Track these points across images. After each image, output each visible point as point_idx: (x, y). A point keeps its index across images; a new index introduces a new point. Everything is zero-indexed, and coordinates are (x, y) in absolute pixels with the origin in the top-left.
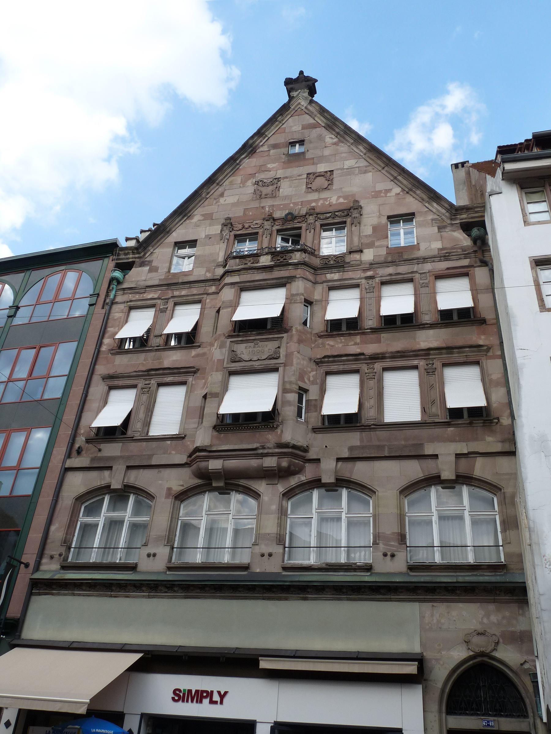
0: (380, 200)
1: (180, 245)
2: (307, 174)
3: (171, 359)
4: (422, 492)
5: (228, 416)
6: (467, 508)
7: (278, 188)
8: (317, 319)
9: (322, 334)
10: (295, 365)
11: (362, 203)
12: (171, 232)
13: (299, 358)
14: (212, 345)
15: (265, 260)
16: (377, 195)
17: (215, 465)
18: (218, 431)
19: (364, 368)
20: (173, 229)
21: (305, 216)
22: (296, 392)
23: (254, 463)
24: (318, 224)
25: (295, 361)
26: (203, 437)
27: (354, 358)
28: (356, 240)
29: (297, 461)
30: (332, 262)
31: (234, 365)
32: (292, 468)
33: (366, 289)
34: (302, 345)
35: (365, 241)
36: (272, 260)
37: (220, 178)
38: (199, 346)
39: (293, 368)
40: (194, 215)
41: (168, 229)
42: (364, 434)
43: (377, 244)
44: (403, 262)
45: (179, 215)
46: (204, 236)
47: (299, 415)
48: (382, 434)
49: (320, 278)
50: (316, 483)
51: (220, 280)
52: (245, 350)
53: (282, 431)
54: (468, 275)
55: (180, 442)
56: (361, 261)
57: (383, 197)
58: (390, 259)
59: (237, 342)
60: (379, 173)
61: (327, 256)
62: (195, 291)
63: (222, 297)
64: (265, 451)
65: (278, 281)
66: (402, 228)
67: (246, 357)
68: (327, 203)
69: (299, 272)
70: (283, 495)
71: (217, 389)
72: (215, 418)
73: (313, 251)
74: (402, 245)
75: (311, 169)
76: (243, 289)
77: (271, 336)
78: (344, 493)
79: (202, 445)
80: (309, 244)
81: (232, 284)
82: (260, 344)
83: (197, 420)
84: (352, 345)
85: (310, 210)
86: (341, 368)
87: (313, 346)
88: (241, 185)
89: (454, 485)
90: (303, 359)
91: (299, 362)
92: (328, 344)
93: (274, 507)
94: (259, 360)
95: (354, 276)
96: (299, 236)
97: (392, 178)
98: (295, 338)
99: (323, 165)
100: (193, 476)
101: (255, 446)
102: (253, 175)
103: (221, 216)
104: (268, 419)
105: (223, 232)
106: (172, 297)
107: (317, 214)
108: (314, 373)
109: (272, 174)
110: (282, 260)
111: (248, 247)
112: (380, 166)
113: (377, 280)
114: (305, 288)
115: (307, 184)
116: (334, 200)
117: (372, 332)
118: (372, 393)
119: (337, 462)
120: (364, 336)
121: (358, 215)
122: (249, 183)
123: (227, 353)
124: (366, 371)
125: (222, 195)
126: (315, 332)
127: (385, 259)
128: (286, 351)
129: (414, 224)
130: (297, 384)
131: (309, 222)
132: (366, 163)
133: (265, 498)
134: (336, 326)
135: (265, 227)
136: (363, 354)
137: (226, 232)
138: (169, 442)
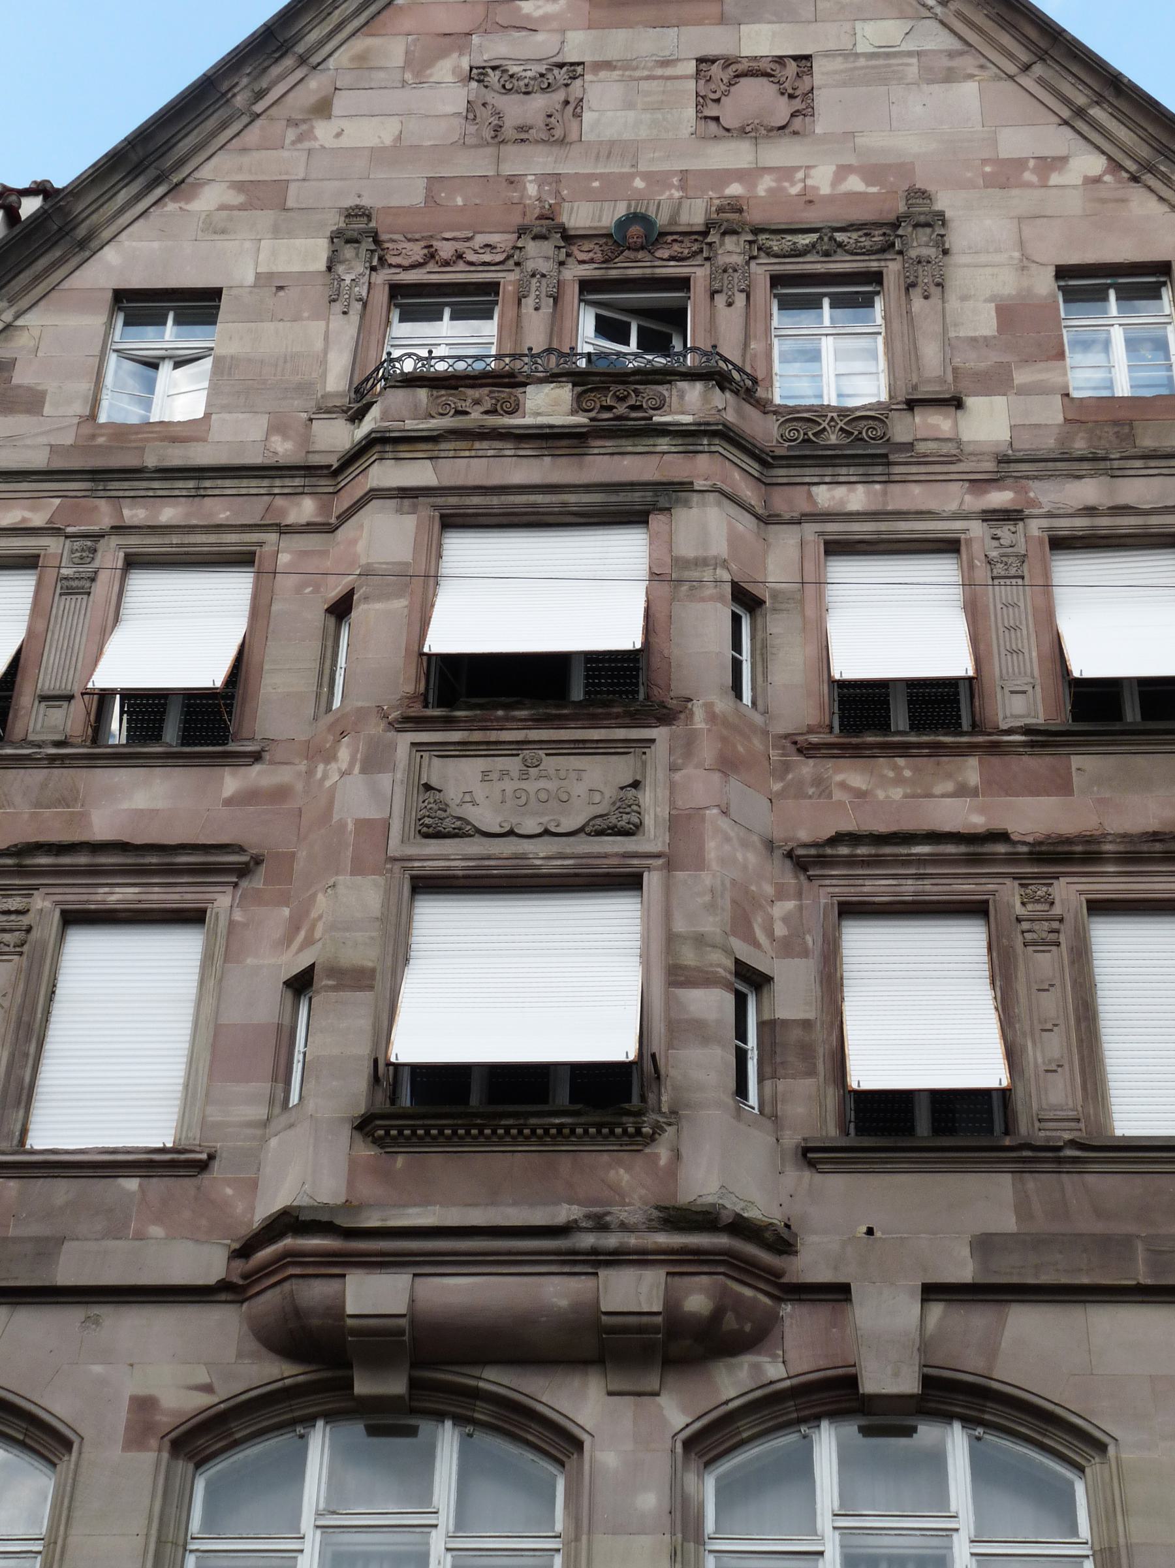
0: (1021, 200)
1: (138, 305)
2: (700, 60)
3: (125, 805)
4: (786, 1440)
5: (407, 1071)
6: (966, 1523)
7: (576, 108)
8: (789, 670)
9: (814, 739)
10: (715, 866)
11: (944, 202)
12: (94, 244)
13: (728, 839)
14: (317, 753)
15: (547, 405)
16: (1005, 175)
17: (373, 1295)
18: (378, 1142)
19: (1009, 895)
20: (106, 234)
21: (705, 234)
22: (728, 986)
23: (557, 1292)
24: (760, 272)
25: (712, 849)
26: (307, 1166)
27: (962, 849)
28: (931, 354)
29: (748, 1292)
30: (833, 439)
31: (434, 847)
32: (730, 1322)
33: (990, 562)
34: (734, 783)
35: (970, 360)
36: (579, 406)
37: (313, 37)
38: (257, 757)
39: (707, 879)
40: (201, 184)
41: (81, 232)
42: (1031, 1183)
43: (1021, 377)
44: (1138, 463)
45: (135, 172)
46: (250, 279)
47: (741, 1090)
48: (1111, 1186)
49: (787, 501)
50: (834, 1395)
51: (336, 473)
52: (477, 786)
53: (677, 1155)
54: (957, 551)
55: (185, 1186)
56: (958, 442)
57: (1029, 185)
58: (1080, 445)
59: (443, 750)
60: (1009, 85)
61: (809, 409)
62: (220, 511)
63: (360, 547)
64: (611, 1241)
65: (613, 498)
66: (1114, 320)
67: (486, 817)
68: (795, 190)
69: (704, 468)
70: (688, 1444)
71: (361, 951)
72: (360, 1084)
73: (749, 383)
74: (1123, 389)
75: (715, 41)
76: (453, 522)
77: (595, 734)
78: (956, 1444)
79: (304, 1201)
80: (730, 350)
81: (406, 494)
82: (551, 763)
83: (263, 1087)
84: (949, 797)
85: (720, 210)
86: (909, 889)
87: (777, 787)
88: (408, 76)
89: (910, 1421)
90: (745, 844)
91: (730, 854)
92: (843, 785)
93: (650, 1501)
94: (547, 832)
95: (932, 505)
96: (676, 318)
97: (1066, 113)
98: (707, 751)
99: (765, 29)
100: (253, 1345)
101: (563, 1214)
102: (459, 40)
103: (335, 196)
104: (603, 1101)
105: (340, 269)
106: (120, 529)
107: (757, 231)
108: (790, 905)
109: (543, 44)
110: (621, 409)
111: (451, 340)
112: (1011, 56)
113: (1035, 527)
114: (734, 540)
115: (701, 100)
116: (822, 179)
117: (1032, 744)
118: (1050, 1004)
119: (923, 1301)
120: (995, 760)
121: (931, 252)
122: (445, 70)
123: (399, 792)
124: (1019, 910)
125: (323, 109)
126: (780, 728)
127: (1064, 439)
128: (672, 803)
129: (879, 320)
130: (728, 951)
131: (722, 260)
132: (946, 41)
133: (606, 1457)
134: (868, 713)
135: (530, 266)
136: (1002, 837)
137: (353, 270)
138: (132, 1184)
